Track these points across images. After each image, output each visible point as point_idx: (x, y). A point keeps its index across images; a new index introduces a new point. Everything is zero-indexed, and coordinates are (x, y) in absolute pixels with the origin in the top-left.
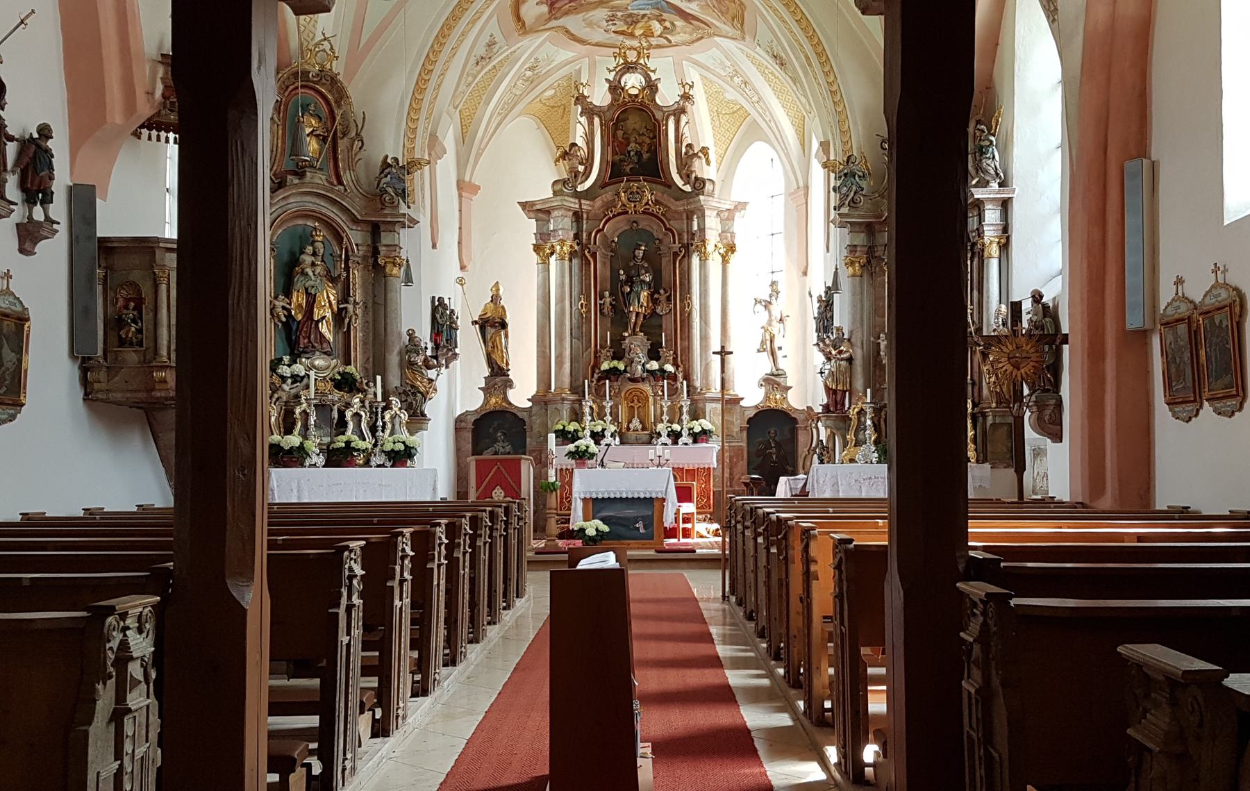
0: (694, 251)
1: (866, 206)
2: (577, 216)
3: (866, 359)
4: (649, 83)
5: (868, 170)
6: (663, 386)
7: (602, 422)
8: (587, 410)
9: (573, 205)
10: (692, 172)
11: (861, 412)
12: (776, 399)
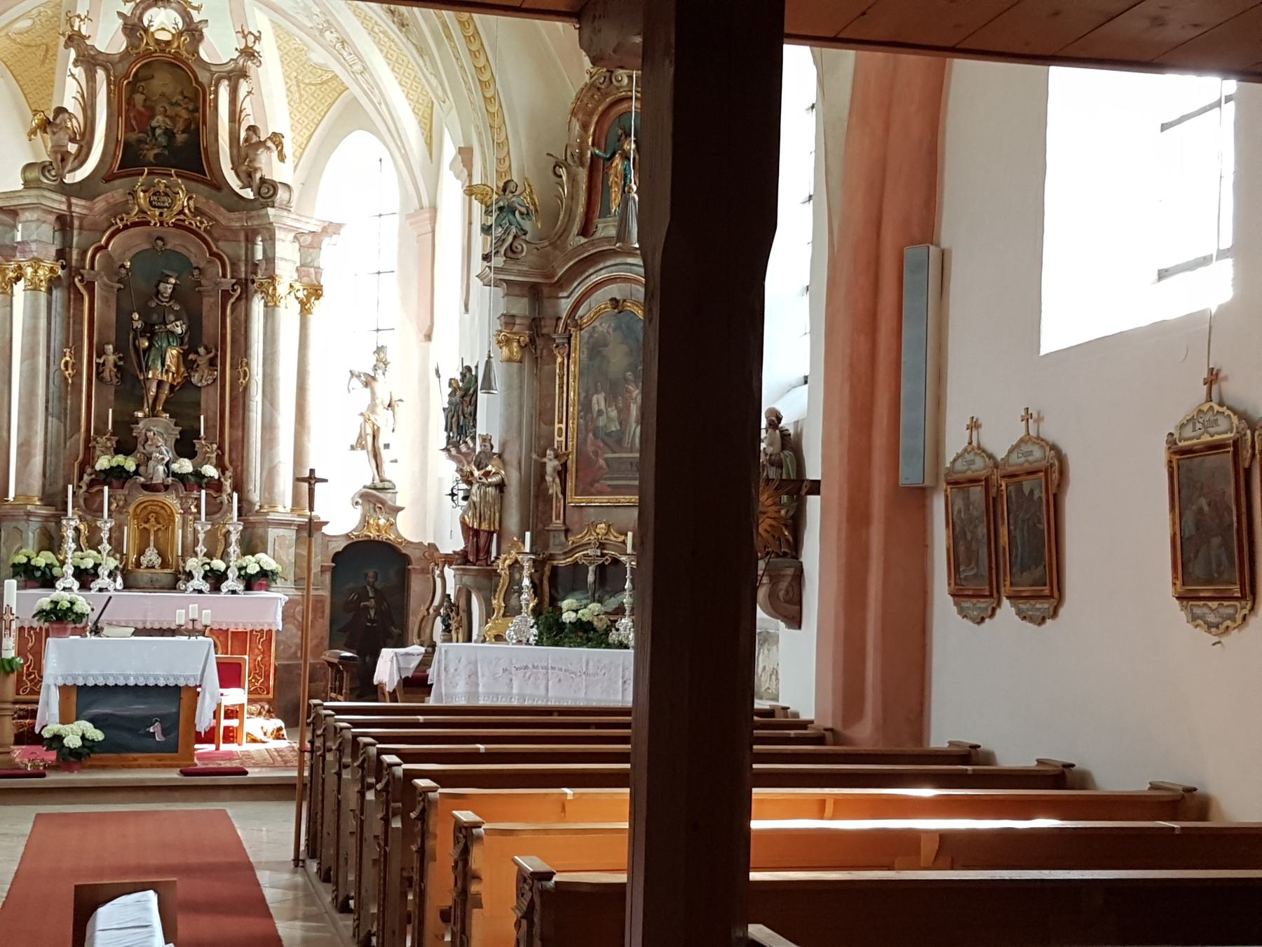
0: (256, 292)
1: (530, 258)
2: (63, 223)
3: (524, 485)
4: (188, 25)
5: (534, 204)
6: (198, 499)
7: (94, 553)
8: (70, 534)
9: (56, 205)
10: (256, 170)
11: (515, 566)
12: (378, 525)
